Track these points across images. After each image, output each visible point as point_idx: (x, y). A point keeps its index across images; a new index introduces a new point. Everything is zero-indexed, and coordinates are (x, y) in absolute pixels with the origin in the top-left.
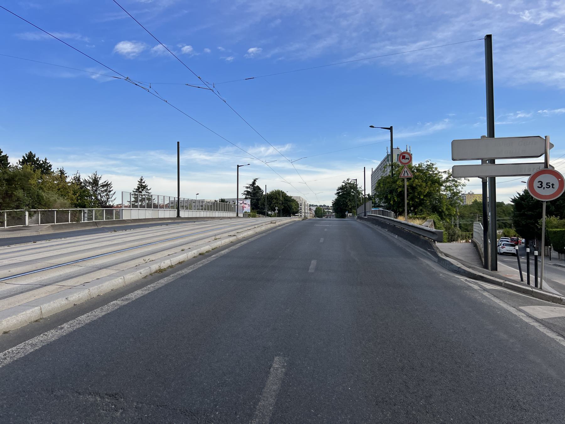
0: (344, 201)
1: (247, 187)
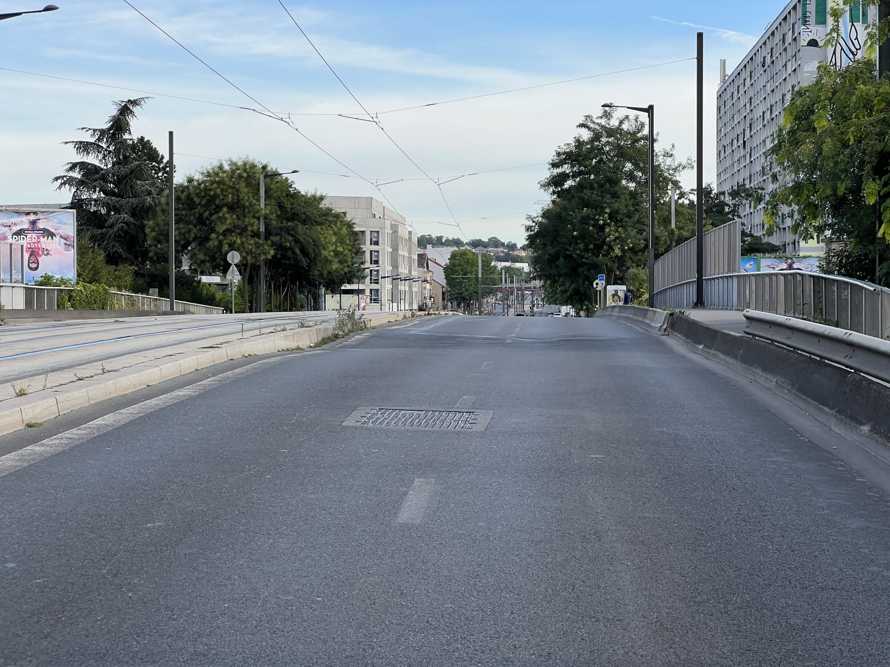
0: (585, 220)
1: (84, 147)
